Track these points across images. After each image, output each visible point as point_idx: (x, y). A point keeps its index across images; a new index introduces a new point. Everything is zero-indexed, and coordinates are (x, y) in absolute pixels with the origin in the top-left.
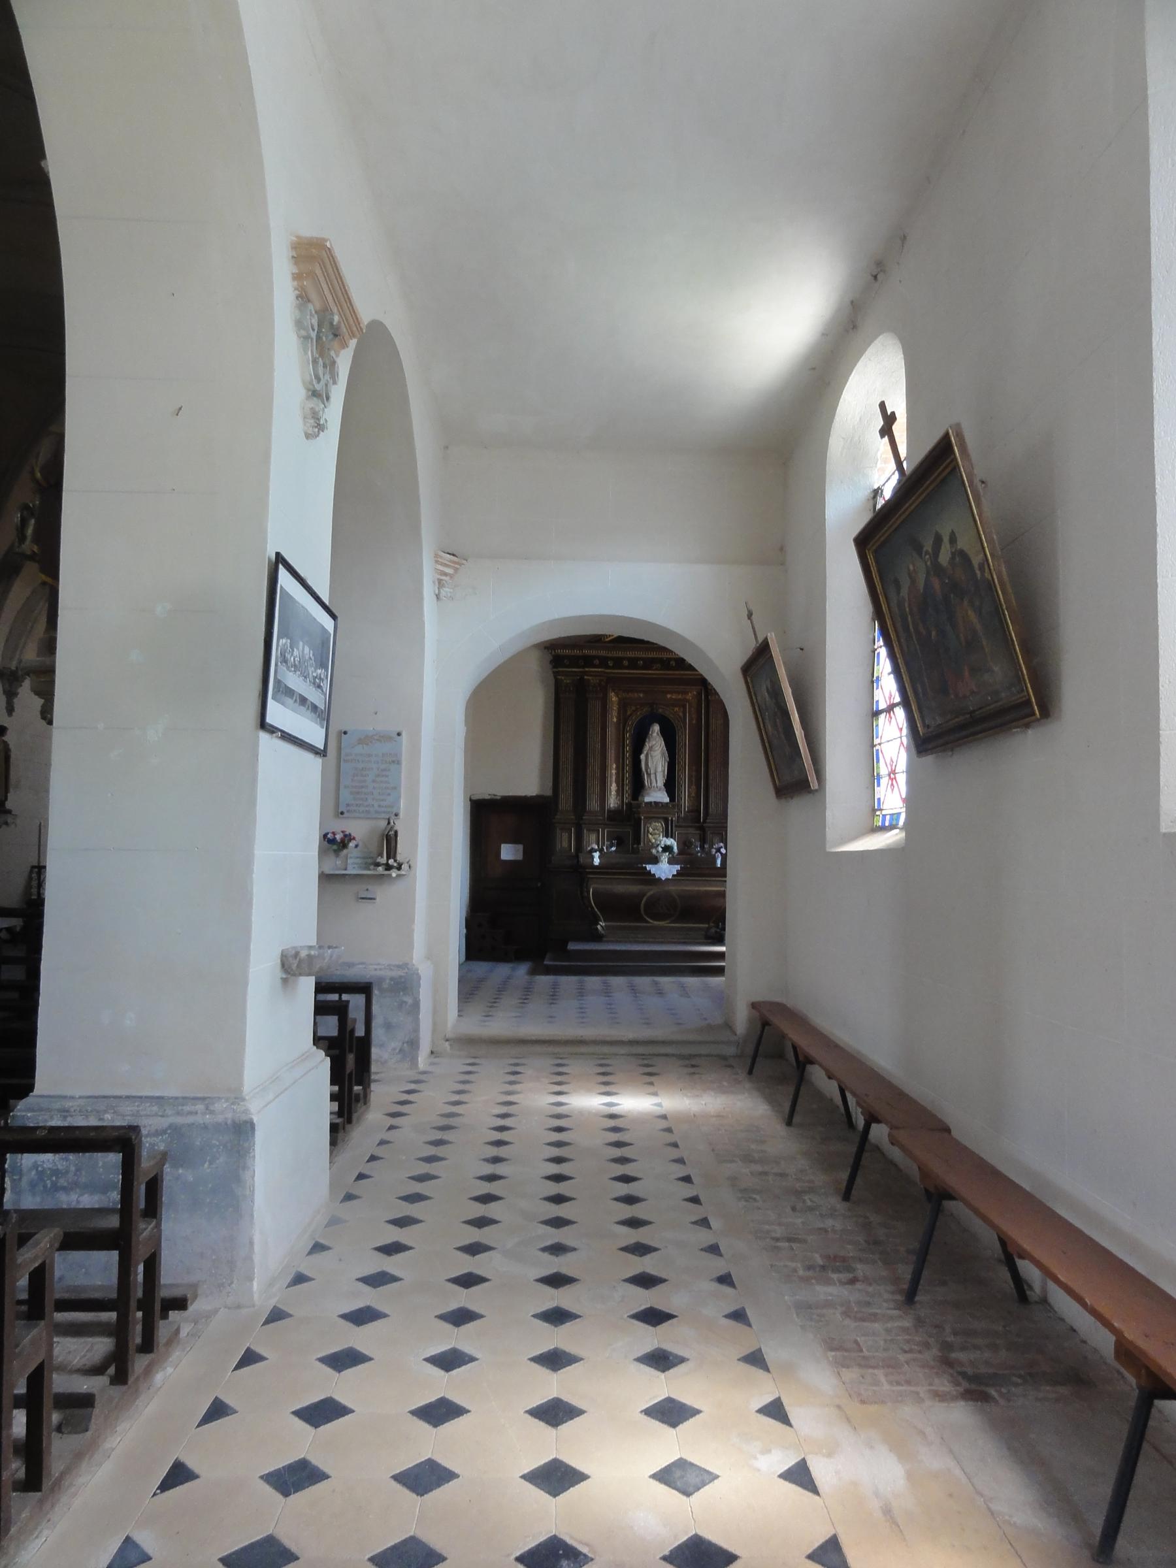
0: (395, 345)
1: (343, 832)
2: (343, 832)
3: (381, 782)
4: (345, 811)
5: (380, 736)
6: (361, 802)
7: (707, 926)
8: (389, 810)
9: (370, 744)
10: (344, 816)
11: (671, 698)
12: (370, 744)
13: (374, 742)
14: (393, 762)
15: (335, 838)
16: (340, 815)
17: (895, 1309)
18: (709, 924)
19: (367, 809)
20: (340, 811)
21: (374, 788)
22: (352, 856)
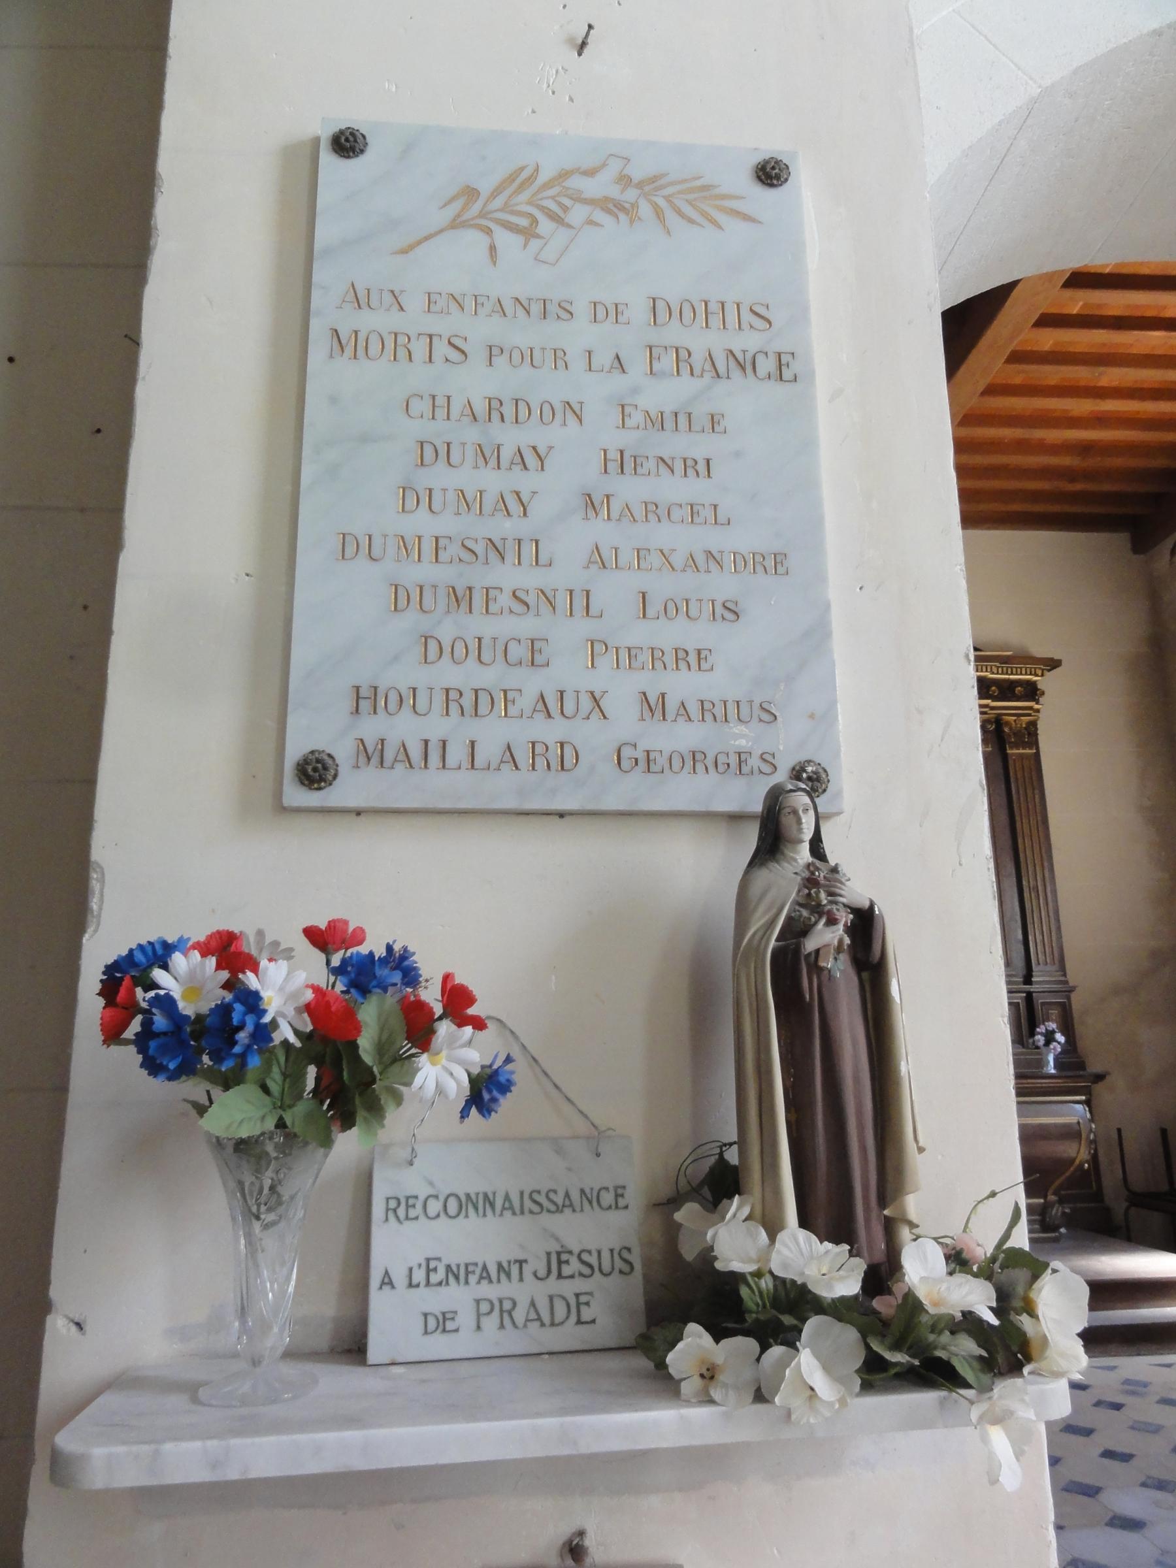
0: (318, 164)
1: (320, 938)
2: (320, 938)
3: (652, 509)
4: (343, 752)
5: (624, 180)
6: (489, 676)
7: (1042, 1201)
8: (741, 737)
9: (545, 226)
10: (332, 796)
11: (289, 1394)
12: (545, 226)
13: (578, 214)
14: (746, 365)
15: (252, 1002)
16: (297, 796)
17: (577, 1543)
18: (1045, 1197)
19: (550, 732)
20: (294, 752)
21: (598, 559)
22: (412, 1182)
